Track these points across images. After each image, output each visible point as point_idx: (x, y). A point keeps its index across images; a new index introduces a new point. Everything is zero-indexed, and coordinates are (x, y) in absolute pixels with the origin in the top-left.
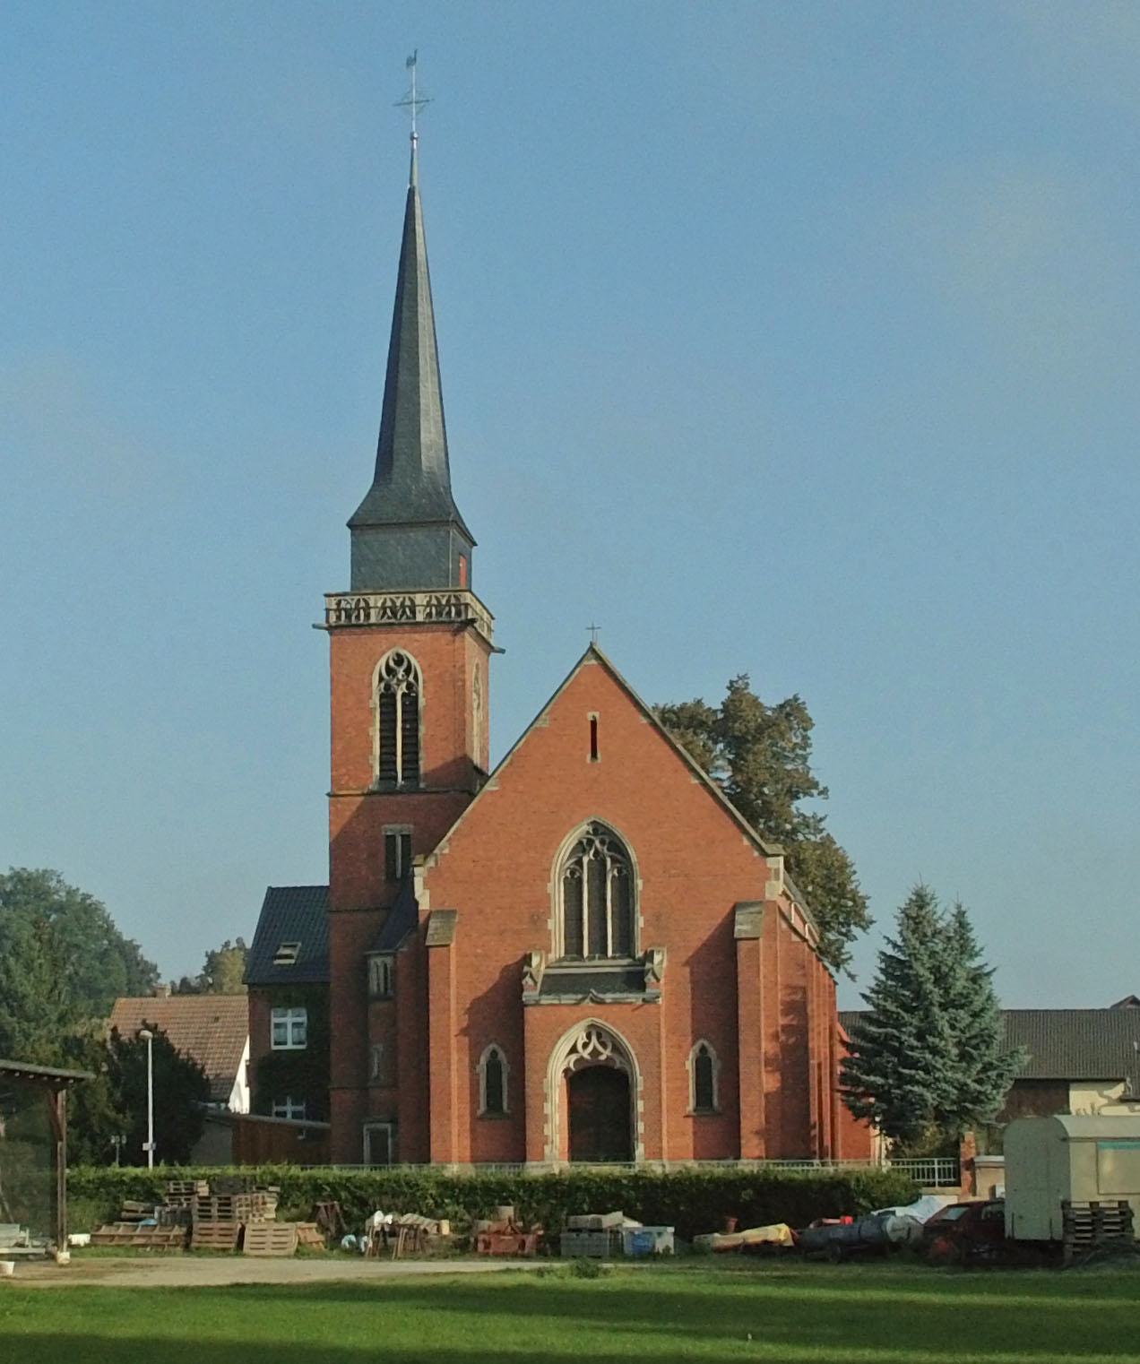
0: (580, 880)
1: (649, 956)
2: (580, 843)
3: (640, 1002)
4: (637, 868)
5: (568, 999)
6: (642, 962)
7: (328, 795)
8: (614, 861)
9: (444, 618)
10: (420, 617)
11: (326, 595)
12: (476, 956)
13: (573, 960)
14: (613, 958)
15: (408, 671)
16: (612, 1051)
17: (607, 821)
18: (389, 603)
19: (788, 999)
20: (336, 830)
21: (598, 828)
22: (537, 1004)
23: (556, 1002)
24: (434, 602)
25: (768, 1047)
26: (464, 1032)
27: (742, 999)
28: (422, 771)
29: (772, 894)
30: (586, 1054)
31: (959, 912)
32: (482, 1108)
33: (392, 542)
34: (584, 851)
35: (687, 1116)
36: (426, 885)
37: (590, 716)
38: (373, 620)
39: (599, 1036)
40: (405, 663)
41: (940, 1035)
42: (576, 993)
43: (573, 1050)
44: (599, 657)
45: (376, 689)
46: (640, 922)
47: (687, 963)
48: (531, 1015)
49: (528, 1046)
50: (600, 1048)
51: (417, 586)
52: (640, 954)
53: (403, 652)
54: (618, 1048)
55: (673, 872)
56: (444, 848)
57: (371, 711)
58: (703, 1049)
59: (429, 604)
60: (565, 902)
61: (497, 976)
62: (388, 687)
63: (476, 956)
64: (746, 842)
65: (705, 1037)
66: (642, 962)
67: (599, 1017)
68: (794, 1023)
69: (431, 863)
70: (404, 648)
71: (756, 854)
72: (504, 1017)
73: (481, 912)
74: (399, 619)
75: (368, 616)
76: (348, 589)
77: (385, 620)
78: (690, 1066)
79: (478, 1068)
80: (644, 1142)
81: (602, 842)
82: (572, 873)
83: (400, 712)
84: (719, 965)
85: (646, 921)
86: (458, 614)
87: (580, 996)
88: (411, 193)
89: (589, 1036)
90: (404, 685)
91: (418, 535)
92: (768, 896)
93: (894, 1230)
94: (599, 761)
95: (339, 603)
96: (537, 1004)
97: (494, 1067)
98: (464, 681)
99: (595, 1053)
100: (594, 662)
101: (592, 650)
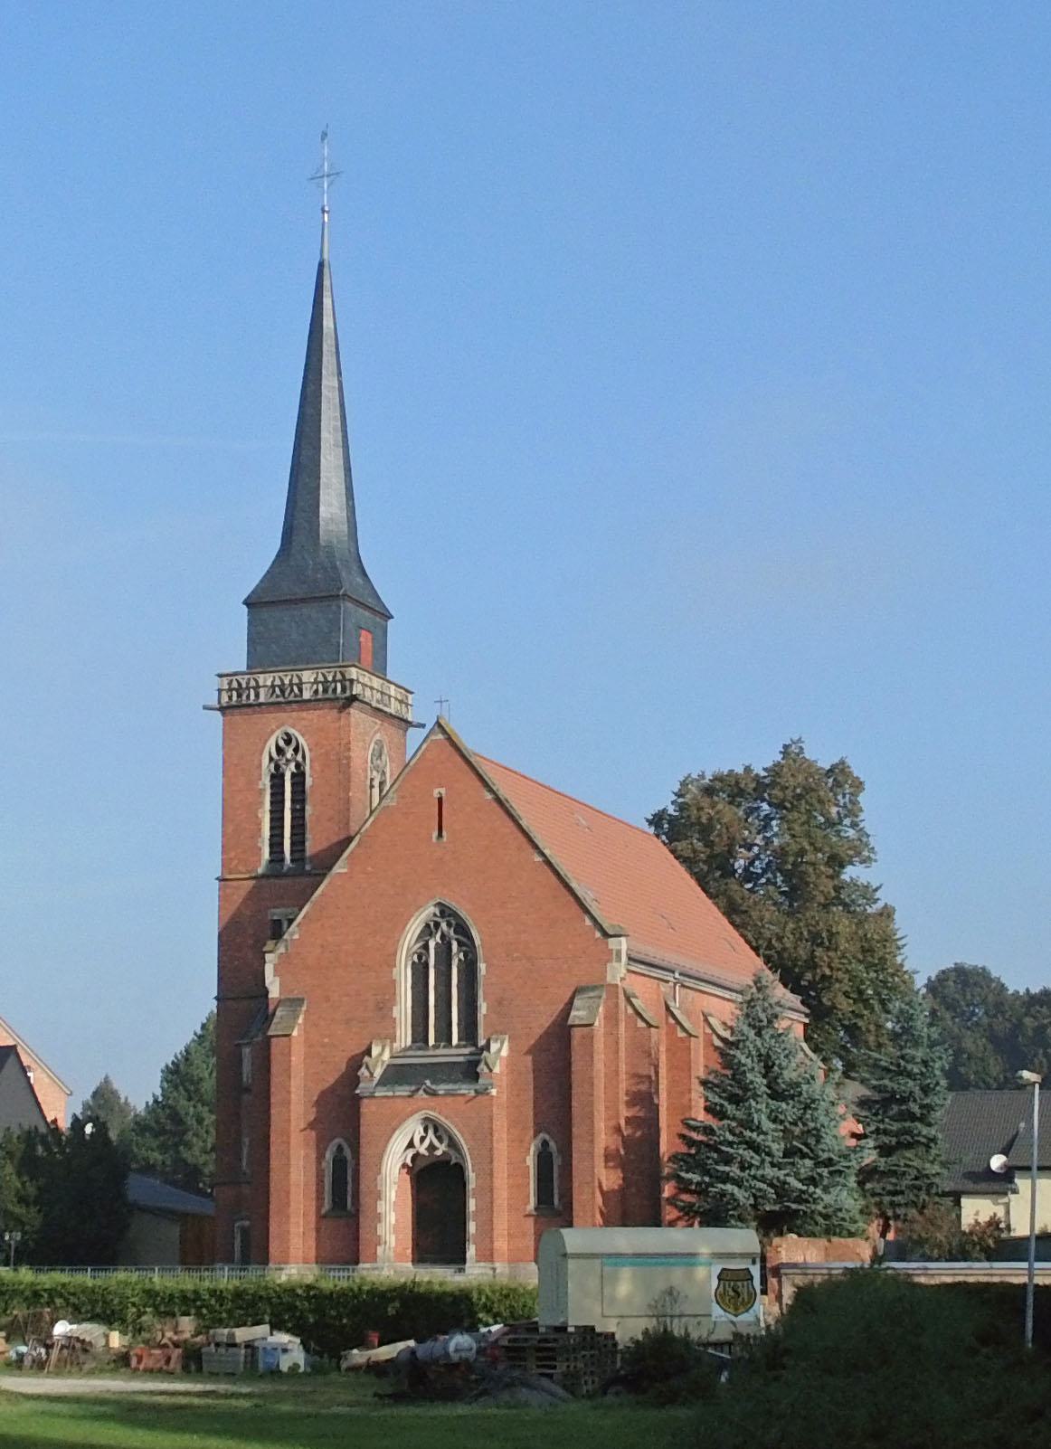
0: (426, 965)
1: (487, 1047)
2: (427, 926)
3: (472, 1093)
4: (480, 952)
5: (403, 1091)
6: (482, 1049)
7: (221, 880)
8: (460, 944)
9: (330, 695)
10: (307, 695)
11: (220, 676)
14: (458, 1046)
15: (296, 750)
16: (449, 1146)
18: (278, 682)
19: (634, 1089)
20: (226, 919)
21: (445, 911)
22: (372, 1097)
24: (321, 678)
25: (604, 1139)
26: (311, 1126)
28: (308, 853)
30: (422, 1150)
32: (327, 1206)
34: (431, 935)
35: (528, 1216)
36: (276, 972)
37: (436, 793)
38: (262, 699)
39: (436, 1131)
40: (294, 744)
41: (759, 1129)
43: (411, 1145)
44: (444, 731)
45: (266, 768)
46: (483, 1008)
47: (528, 1052)
48: (367, 1108)
49: (362, 1141)
50: (436, 1143)
51: (308, 661)
52: (482, 1042)
53: (291, 731)
54: (453, 1144)
56: (293, 933)
57: (261, 792)
58: (545, 1144)
59: (316, 682)
61: (343, 1067)
62: (277, 767)
63: (323, 1046)
64: (588, 922)
66: (482, 1049)
67: (433, 1109)
68: (641, 1114)
69: (282, 949)
71: (598, 934)
72: (342, 1115)
73: (328, 999)
74: (287, 700)
75: (257, 695)
76: (244, 669)
77: (273, 699)
78: (531, 1161)
79: (324, 1164)
81: (449, 925)
82: (420, 957)
83: (290, 790)
84: (555, 1058)
86: (344, 690)
88: (321, 265)
89: (426, 1130)
90: (292, 765)
91: (309, 611)
92: (609, 979)
93: (457, 1350)
95: (230, 683)
96: (372, 1097)
97: (339, 1163)
98: (349, 758)
99: (432, 1148)
100: (440, 736)
101: (438, 724)
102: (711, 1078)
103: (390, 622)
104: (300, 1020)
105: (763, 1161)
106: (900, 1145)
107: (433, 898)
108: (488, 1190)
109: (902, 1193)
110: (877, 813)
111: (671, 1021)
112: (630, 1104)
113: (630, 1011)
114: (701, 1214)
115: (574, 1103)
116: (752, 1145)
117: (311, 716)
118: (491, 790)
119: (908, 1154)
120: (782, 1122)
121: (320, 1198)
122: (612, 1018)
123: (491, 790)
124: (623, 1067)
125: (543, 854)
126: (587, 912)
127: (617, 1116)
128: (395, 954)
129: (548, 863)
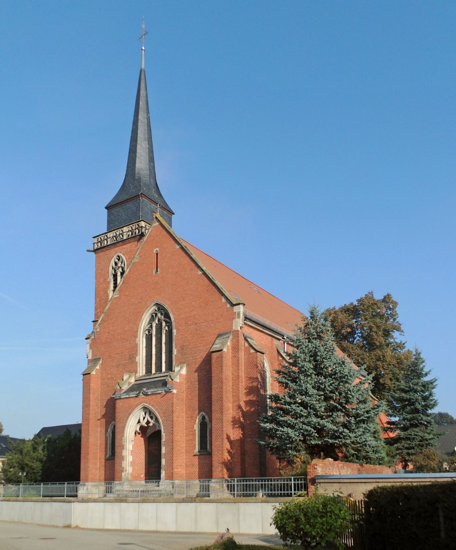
0: (151, 335)
2: (152, 316)
4: (174, 324)
8: (166, 322)
9: (134, 235)
11: (94, 237)
12: (108, 379)
13: (149, 375)
14: (164, 373)
17: (161, 303)
23: (127, 396)
24: (130, 229)
26: (103, 416)
27: (214, 386)
29: (236, 326)
31: (417, 353)
33: (121, 211)
38: (109, 243)
41: (306, 394)
42: (136, 391)
43: (139, 422)
45: (111, 271)
46: (175, 352)
50: (150, 420)
54: (157, 419)
55: (189, 323)
57: (109, 283)
58: (204, 418)
60: (146, 347)
64: (224, 300)
65: (204, 411)
70: (120, 252)
71: (228, 306)
78: (197, 427)
80: (165, 470)
81: (162, 314)
82: (149, 332)
85: (177, 351)
87: (137, 392)
89: (145, 414)
91: (129, 205)
92: (234, 328)
94: (159, 272)
96: (120, 399)
99: (148, 422)
100: (157, 224)
102: (282, 370)
103: (173, 216)
104: (98, 367)
105: (309, 413)
106: (412, 426)
107: (153, 301)
108: (171, 441)
109: (413, 448)
110: (403, 315)
111: (281, 358)
112: (248, 394)
113: (247, 345)
114: (244, 440)
115: (213, 394)
116: (304, 405)
117: (127, 246)
118: (179, 244)
119: (416, 430)
120: (323, 390)
121: (106, 451)
122: (236, 348)
123: (179, 244)
124: (242, 374)
125: (202, 270)
126: (223, 295)
127: (239, 400)
128: (137, 331)
129: (205, 274)
